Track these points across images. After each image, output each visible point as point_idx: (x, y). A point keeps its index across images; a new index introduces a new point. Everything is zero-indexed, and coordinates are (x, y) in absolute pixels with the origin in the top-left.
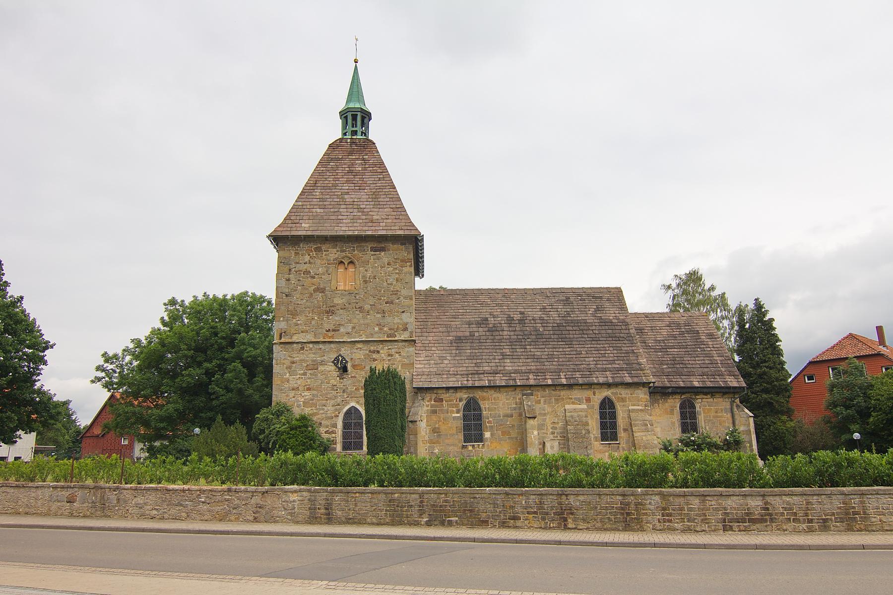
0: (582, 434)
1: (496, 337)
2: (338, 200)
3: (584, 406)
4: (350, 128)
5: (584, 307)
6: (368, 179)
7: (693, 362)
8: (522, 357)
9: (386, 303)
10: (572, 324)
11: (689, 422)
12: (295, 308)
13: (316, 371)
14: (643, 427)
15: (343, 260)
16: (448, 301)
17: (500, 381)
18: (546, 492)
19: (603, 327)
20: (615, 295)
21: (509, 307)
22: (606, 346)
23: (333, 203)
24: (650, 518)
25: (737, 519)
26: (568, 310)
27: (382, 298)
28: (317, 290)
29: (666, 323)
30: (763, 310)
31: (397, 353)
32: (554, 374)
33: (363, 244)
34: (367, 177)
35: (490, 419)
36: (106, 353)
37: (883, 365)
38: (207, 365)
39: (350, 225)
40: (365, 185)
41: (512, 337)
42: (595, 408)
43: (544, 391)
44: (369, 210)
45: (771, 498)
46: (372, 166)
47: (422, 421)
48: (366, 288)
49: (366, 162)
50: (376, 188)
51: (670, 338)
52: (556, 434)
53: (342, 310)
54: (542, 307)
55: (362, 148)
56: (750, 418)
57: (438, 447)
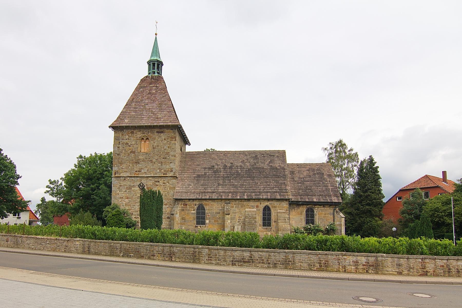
0: (252, 223)
1: (217, 175)
2: (143, 108)
3: (255, 210)
4: (152, 71)
5: (264, 160)
6: (157, 97)
7: (316, 189)
8: (228, 185)
9: (163, 159)
10: (256, 169)
11: (310, 218)
12: (121, 161)
13: (131, 190)
14: (284, 221)
15: (144, 138)
16: (197, 157)
17: (214, 196)
18: (165, 245)
19: (272, 171)
20: (281, 154)
21: (226, 161)
22: (271, 180)
23: (140, 109)
24: (203, 258)
25: (238, 261)
26: (255, 162)
27: (161, 156)
28: (132, 152)
29: (308, 169)
30: (374, 162)
31: (167, 182)
32: (241, 194)
33: (153, 130)
34: (157, 95)
35: (209, 214)
36: (50, 180)
37: (439, 192)
38: (92, 186)
39: (147, 120)
40: (156, 100)
41: (225, 175)
42: (260, 211)
43: (236, 202)
44: (156, 113)
45: (253, 252)
46: (160, 90)
47: (177, 214)
48: (154, 151)
49: (158, 88)
50: (161, 101)
51: (308, 177)
52: (240, 222)
53: (143, 162)
54: (242, 160)
55: (156, 80)
56: (342, 218)
57: (184, 226)
